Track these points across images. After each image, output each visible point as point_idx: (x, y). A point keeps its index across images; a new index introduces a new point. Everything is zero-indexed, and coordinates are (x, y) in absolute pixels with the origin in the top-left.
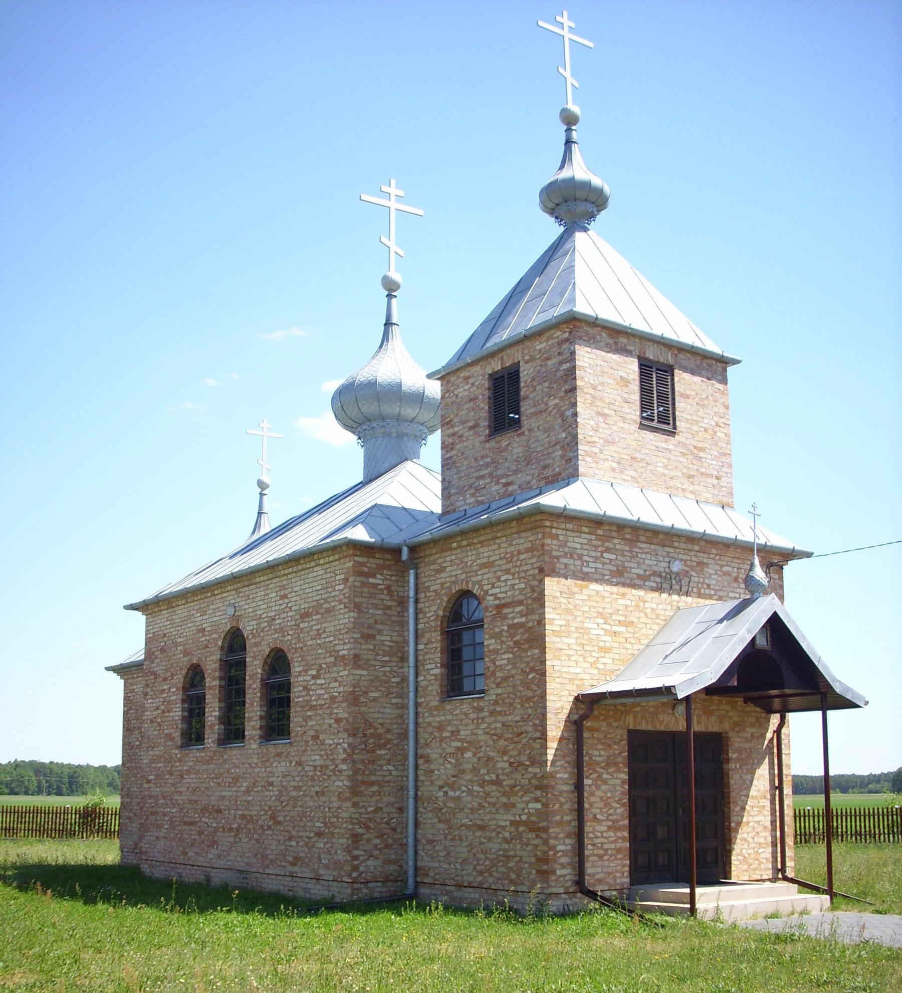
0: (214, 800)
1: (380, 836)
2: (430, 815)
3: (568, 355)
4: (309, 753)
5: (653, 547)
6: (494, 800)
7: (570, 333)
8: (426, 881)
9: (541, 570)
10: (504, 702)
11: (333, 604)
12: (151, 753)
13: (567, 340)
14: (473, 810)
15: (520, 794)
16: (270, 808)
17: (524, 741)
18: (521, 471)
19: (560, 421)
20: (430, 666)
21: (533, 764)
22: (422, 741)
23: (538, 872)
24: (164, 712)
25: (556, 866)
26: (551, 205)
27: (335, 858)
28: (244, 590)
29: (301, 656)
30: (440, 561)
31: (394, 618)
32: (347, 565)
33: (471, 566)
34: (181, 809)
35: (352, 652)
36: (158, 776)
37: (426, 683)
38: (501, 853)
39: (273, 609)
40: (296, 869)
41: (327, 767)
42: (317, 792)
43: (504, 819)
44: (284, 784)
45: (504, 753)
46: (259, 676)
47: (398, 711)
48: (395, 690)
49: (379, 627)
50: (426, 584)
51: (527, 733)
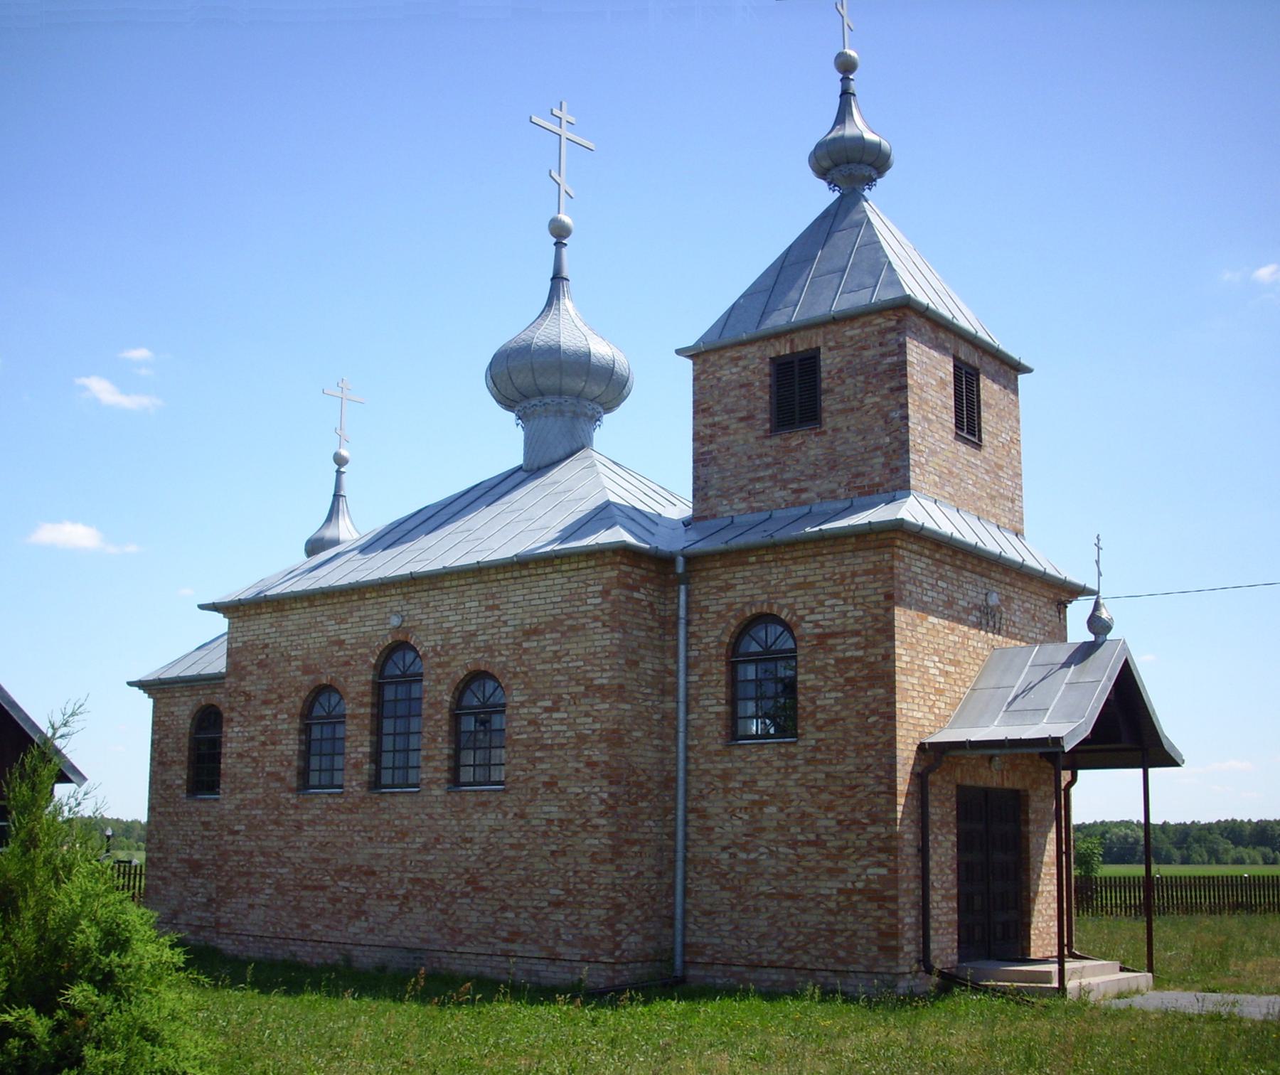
0: (361, 859)
1: (640, 907)
2: (707, 881)
3: (896, 346)
4: (539, 803)
5: (974, 576)
6: (812, 864)
7: (898, 322)
8: (700, 960)
9: (889, 597)
10: (828, 748)
11: (583, 621)
12: (239, 796)
13: (893, 329)
14: (778, 876)
15: (854, 857)
16: (467, 870)
17: (860, 796)
18: (821, 477)
19: (881, 422)
20: (707, 702)
21: (874, 822)
22: (694, 792)
23: (881, 948)
24: (264, 744)
25: (904, 942)
26: (826, 164)
27: (585, 932)
28: (417, 595)
29: (524, 683)
30: (725, 576)
31: (656, 642)
32: (606, 575)
33: (775, 586)
34: (296, 870)
35: (617, 681)
36: (250, 827)
37: (700, 722)
38: (823, 926)
39: (474, 621)
40: (515, 947)
41: (571, 821)
42: (553, 853)
43: (829, 886)
44: (492, 840)
45: (830, 808)
46: (447, 705)
47: (659, 755)
48: (656, 729)
49: (642, 652)
50: (703, 604)
51: (866, 786)
